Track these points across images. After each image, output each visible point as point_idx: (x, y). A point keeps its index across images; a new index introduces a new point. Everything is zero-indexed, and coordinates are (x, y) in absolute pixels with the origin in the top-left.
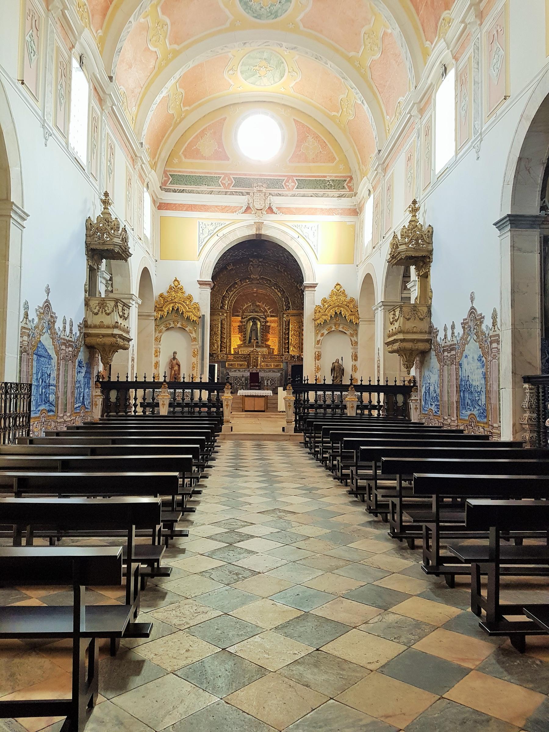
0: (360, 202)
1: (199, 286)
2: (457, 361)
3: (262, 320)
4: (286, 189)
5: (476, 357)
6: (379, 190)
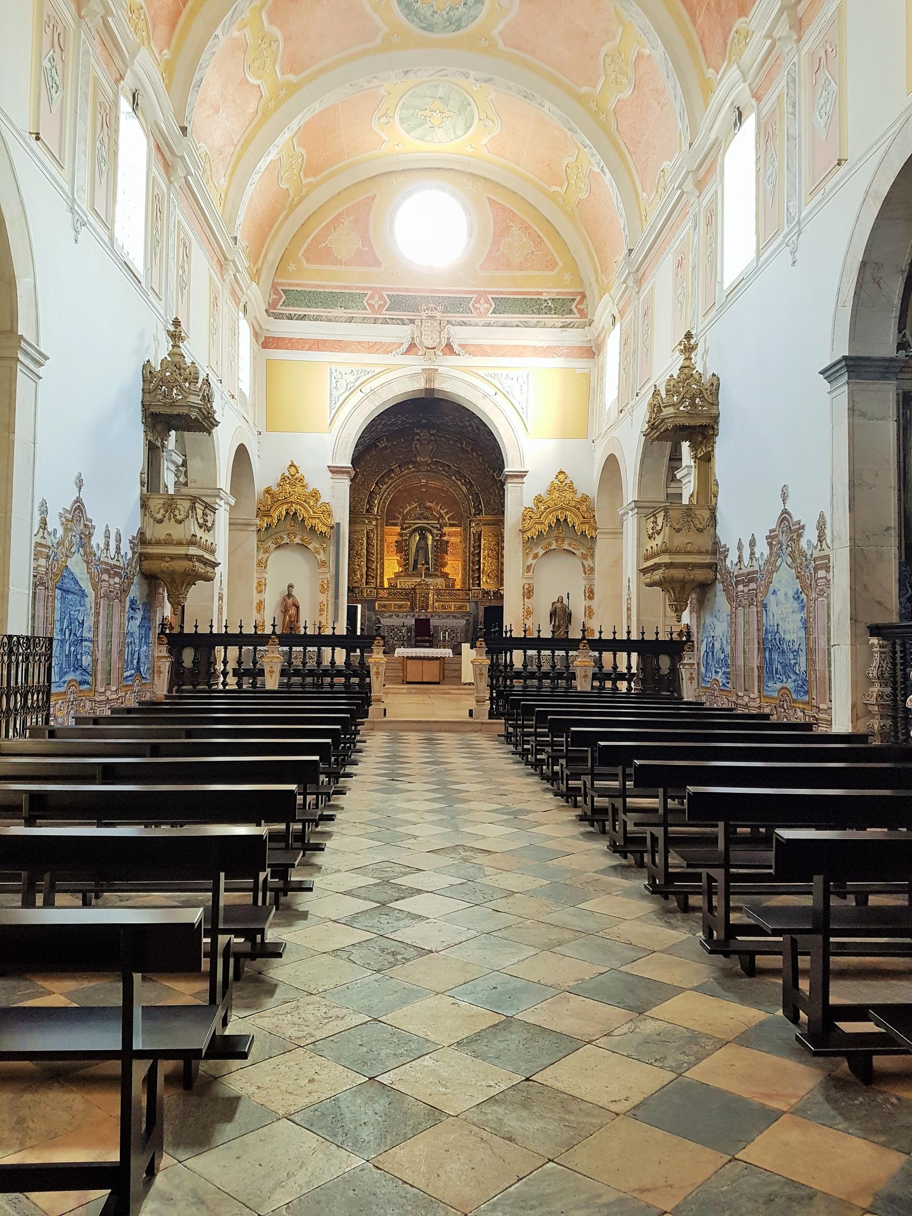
0: (598, 336)
1: (330, 475)
2: (759, 599)
3: (436, 532)
4: (474, 314)
5: (791, 593)
6: (629, 315)
